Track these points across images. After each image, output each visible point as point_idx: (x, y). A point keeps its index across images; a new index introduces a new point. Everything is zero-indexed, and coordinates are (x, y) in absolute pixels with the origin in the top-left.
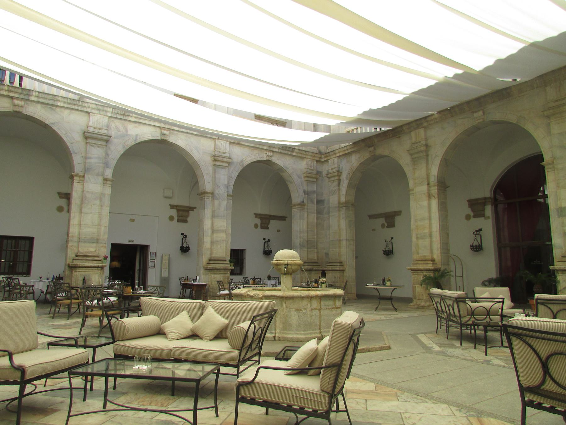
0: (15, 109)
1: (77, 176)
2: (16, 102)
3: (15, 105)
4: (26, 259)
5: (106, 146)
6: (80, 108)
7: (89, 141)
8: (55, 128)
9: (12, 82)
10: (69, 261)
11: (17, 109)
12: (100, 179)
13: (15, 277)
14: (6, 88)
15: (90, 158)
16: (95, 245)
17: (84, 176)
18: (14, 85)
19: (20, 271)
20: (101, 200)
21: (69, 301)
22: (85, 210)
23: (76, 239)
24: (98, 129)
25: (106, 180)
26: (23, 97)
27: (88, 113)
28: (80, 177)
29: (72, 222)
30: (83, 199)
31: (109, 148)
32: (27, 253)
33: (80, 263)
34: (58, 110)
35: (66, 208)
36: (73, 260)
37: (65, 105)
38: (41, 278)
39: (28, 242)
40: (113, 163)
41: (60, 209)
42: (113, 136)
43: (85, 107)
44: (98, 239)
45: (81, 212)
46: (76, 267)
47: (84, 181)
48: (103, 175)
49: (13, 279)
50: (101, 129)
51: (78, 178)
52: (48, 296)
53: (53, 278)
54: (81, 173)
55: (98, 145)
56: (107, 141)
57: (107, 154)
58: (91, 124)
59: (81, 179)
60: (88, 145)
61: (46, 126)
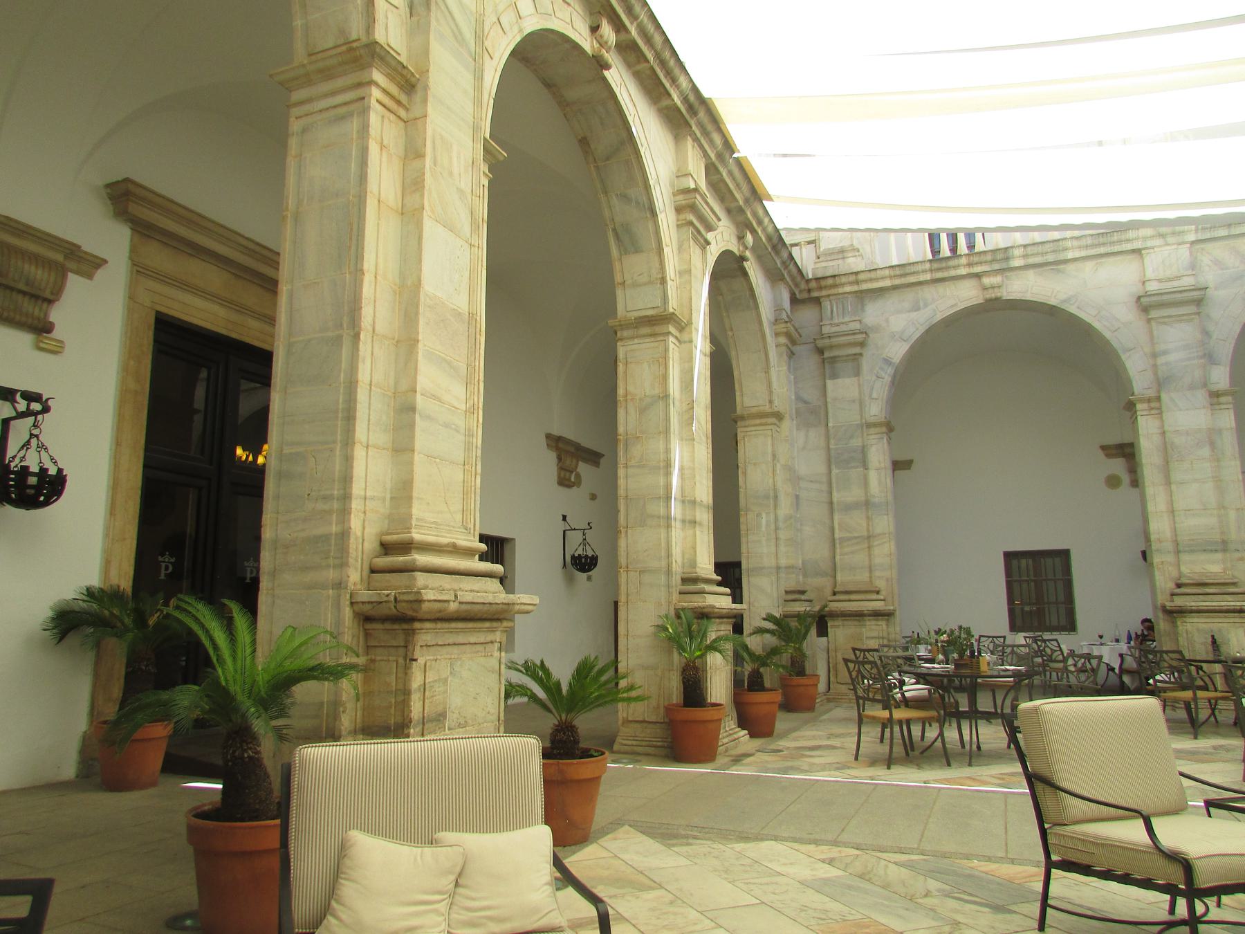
0: (988, 296)
1: (1141, 401)
2: (987, 281)
3: (985, 289)
4: (1061, 598)
5: (1198, 314)
6: (1117, 248)
7: (1154, 314)
8: (1072, 309)
9: (954, 249)
10: (1162, 599)
11: (991, 294)
12: (1201, 396)
13: (1047, 636)
14: (964, 261)
15: (1165, 353)
16: (1219, 556)
17: (1158, 399)
18: (976, 250)
19: (1055, 623)
20: (1212, 444)
21: (1188, 694)
22: (1176, 476)
23: (1169, 546)
24: (1169, 280)
25: (1215, 395)
26: (996, 266)
27: (1137, 252)
28: (1149, 400)
29: (1151, 507)
30: (1166, 449)
31: (1208, 316)
32: (1060, 586)
33: (1191, 603)
34: (1070, 267)
35: (1125, 478)
36: (1172, 595)
37: (1083, 253)
38: (1101, 637)
39: (1058, 560)
40: (1225, 351)
41: (1113, 482)
42: (1211, 285)
43: (1128, 240)
44: (1224, 542)
45: (1168, 482)
46: (1182, 612)
47: (1160, 408)
48: (1205, 385)
49: (1044, 641)
50: (1178, 278)
51: (1145, 406)
52: (1126, 679)
53: (1129, 638)
54: (1151, 393)
55: (1179, 319)
56: (1199, 302)
57: (1206, 333)
58: (1149, 274)
59: (1153, 405)
60: (1153, 323)
61: (1051, 311)
